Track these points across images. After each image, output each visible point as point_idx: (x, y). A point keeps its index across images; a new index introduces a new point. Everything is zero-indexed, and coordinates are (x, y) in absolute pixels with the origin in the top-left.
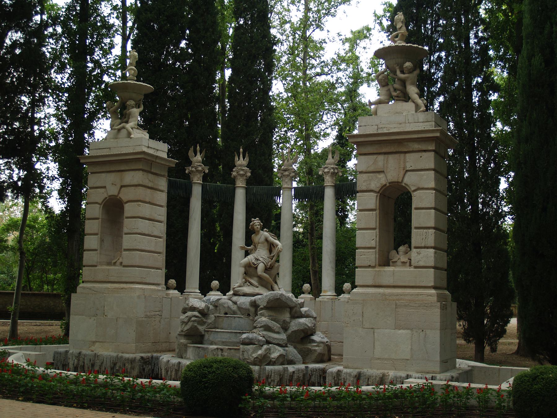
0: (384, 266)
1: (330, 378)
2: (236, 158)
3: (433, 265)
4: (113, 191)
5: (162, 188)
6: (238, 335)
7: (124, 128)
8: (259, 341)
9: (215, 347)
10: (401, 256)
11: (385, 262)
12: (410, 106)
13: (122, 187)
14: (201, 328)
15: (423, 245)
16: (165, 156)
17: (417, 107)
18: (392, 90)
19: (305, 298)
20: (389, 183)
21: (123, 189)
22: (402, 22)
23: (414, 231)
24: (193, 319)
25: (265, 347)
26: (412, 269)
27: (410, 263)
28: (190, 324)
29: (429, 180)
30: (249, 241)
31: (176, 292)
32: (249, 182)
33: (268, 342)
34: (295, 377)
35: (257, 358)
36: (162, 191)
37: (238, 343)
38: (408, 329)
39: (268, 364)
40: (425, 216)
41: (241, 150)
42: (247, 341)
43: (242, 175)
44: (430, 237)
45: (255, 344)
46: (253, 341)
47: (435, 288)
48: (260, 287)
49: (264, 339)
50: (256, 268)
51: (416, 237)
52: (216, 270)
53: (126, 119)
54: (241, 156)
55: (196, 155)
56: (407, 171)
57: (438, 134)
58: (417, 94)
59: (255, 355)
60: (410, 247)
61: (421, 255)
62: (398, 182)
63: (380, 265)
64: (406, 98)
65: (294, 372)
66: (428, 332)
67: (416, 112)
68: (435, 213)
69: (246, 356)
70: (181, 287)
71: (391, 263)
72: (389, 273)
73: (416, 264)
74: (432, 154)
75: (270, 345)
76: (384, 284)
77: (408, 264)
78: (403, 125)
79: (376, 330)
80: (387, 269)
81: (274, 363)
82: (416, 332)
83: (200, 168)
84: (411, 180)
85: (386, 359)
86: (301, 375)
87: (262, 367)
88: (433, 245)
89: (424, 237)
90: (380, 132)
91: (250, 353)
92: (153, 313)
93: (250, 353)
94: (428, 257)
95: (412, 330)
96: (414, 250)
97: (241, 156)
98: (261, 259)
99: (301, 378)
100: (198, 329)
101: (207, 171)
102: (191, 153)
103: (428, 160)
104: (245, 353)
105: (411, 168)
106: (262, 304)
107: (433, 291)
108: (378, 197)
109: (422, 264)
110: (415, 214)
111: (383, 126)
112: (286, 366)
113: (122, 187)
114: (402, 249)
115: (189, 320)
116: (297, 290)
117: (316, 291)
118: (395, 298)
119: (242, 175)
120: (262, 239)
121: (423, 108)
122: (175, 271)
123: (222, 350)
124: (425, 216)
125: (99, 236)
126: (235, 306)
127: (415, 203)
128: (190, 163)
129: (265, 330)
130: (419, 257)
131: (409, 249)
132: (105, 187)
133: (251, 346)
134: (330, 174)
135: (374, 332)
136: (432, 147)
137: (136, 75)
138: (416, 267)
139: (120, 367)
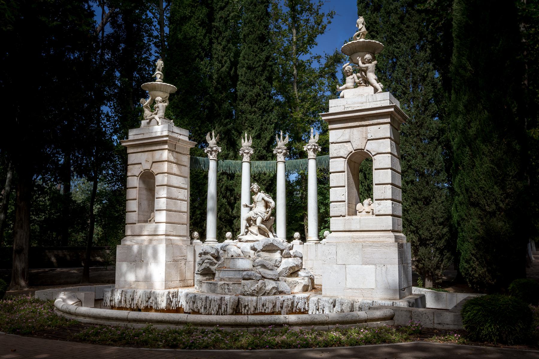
0: (353, 215)
1: (313, 305)
2: (243, 141)
3: (391, 182)
4: (147, 166)
5: (185, 164)
6: (241, 272)
7: (154, 118)
8: (256, 277)
9: (223, 282)
10: (364, 206)
11: (353, 212)
12: (370, 89)
13: (153, 162)
14: (213, 268)
15: (382, 198)
16: (187, 139)
17: (376, 90)
18: (356, 78)
19: (296, 243)
20: (355, 150)
21: (154, 164)
22: (363, 24)
23: (375, 187)
24: (206, 261)
25: (261, 281)
26: (374, 217)
27: (373, 212)
28: (204, 265)
29: (386, 146)
30: (252, 201)
31: (199, 241)
32: (252, 158)
33: (263, 277)
34: (285, 304)
35: (254, 290)
36: (185, 166)
37: (240, 278)
38: (373, 264)
39: (264, 295)
40: (383, 175)
41: (246, 135)
42: (247, 277)
43: (248, 153)
44: (388, 191)
45: (253, 279)
46: (251, 278)
47: (393, 231)
48: (259, 235)
49: (260, 275)
50: (256, 220)
51: (377, 191)
52: (229, 224)
53: (155, 112)
54: (246, 139)
55: (211, 139)
56: (368, 140)
57: (392, 109)
58: (376, 80)
59: (253, 288)
60: (372, 199)
61: (381, 206)
62: (361, 149)
63: (349, 215)
64: (367, 82)
65: (284, 301)
66: (389, 266)
67: (375, 93)
68: (392, 172)
69: (246, 289)
70: (203, 237)
71: (358, 213)
72: (355, 222)
73: (377, 213)
74: (388, 126)
75: (265, 280)
76: (353, 230)
77: (371, 213)
78: (364, 104)
79: (347, 266)
80: (354, 217)
81: (268, 294)
82: (379, 266)
83: (215, 149)
84: (371, 147)
85: (356, 289)
86: (290, 302)
87: (259, 297)
88: (391, 197)
89: (383, 192)
90: (346, 110)
91: (249, 286)
92: (180, 258)
93: (249, 286)
94: (387, 207)
95: (375, 265)
96: (375, 202)
97: (246, 139)
98: (259, 214)
99: (290, 305)
100: (210, 269)
101: (220, 151)
102: (208, 137)
103: (385, 130)
104: (245, 287)
105: (371, 138)
106: (259, 248)
107: (392, 234)
108: (346, 162)
109: (382, 212)
110: (375, 174)
111: (348, 106)
112: (277, 296)
113: (153, 162)
114: (366, 201)
115: (203, 262)
116: (289, 238)
117: (303, 239)
118: (361, 240)
119: (248, 153)
120: (260, 199)
121: (380, 90)
122: (197, 224)
123: (228, 284)
124: (383, 175)
125: (137, 200)
126: (239, 250)
127: (375, 165)
128: (207, 145)
129: (261, 267)
130: (380, 207)
131: (371, 202)
132: (141, 164)
133: (250, 281)
134: (312, 150)
135: (346, 268)
136: (389, 120)
137: (162, 78)
138: (376, 215)
139: (153, 300)
